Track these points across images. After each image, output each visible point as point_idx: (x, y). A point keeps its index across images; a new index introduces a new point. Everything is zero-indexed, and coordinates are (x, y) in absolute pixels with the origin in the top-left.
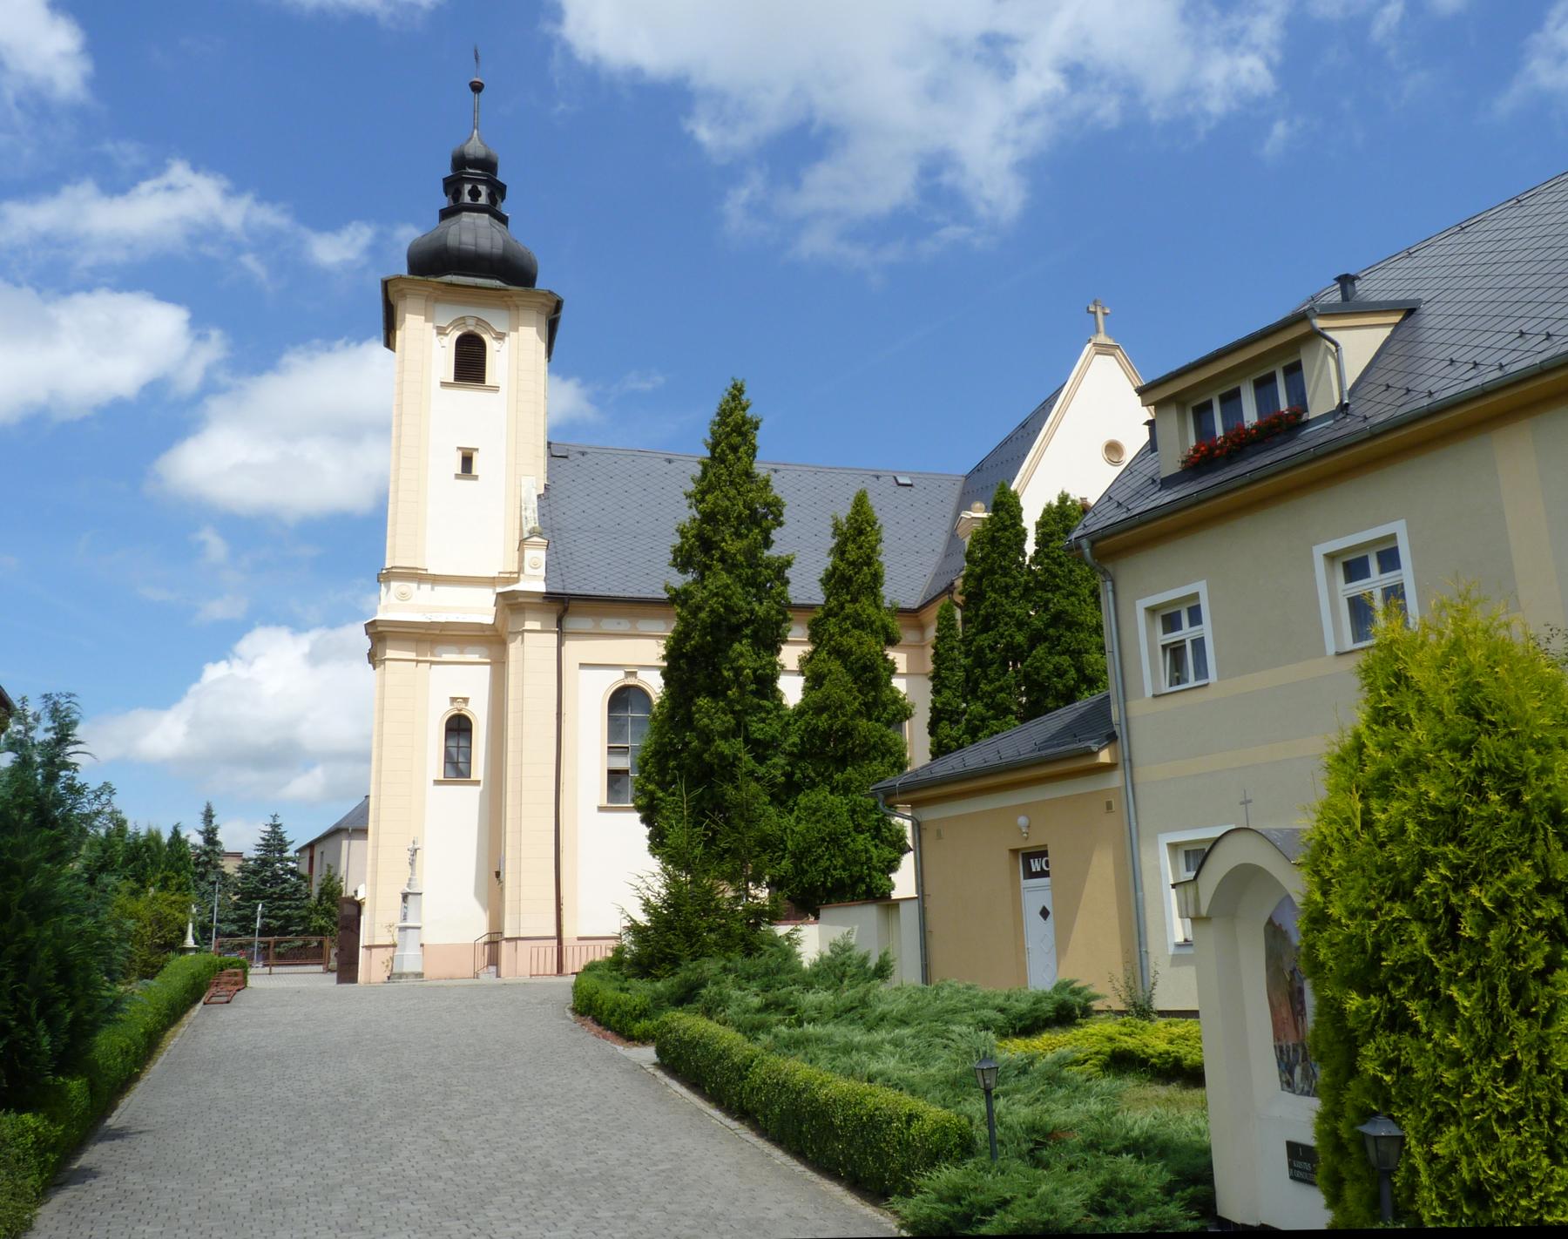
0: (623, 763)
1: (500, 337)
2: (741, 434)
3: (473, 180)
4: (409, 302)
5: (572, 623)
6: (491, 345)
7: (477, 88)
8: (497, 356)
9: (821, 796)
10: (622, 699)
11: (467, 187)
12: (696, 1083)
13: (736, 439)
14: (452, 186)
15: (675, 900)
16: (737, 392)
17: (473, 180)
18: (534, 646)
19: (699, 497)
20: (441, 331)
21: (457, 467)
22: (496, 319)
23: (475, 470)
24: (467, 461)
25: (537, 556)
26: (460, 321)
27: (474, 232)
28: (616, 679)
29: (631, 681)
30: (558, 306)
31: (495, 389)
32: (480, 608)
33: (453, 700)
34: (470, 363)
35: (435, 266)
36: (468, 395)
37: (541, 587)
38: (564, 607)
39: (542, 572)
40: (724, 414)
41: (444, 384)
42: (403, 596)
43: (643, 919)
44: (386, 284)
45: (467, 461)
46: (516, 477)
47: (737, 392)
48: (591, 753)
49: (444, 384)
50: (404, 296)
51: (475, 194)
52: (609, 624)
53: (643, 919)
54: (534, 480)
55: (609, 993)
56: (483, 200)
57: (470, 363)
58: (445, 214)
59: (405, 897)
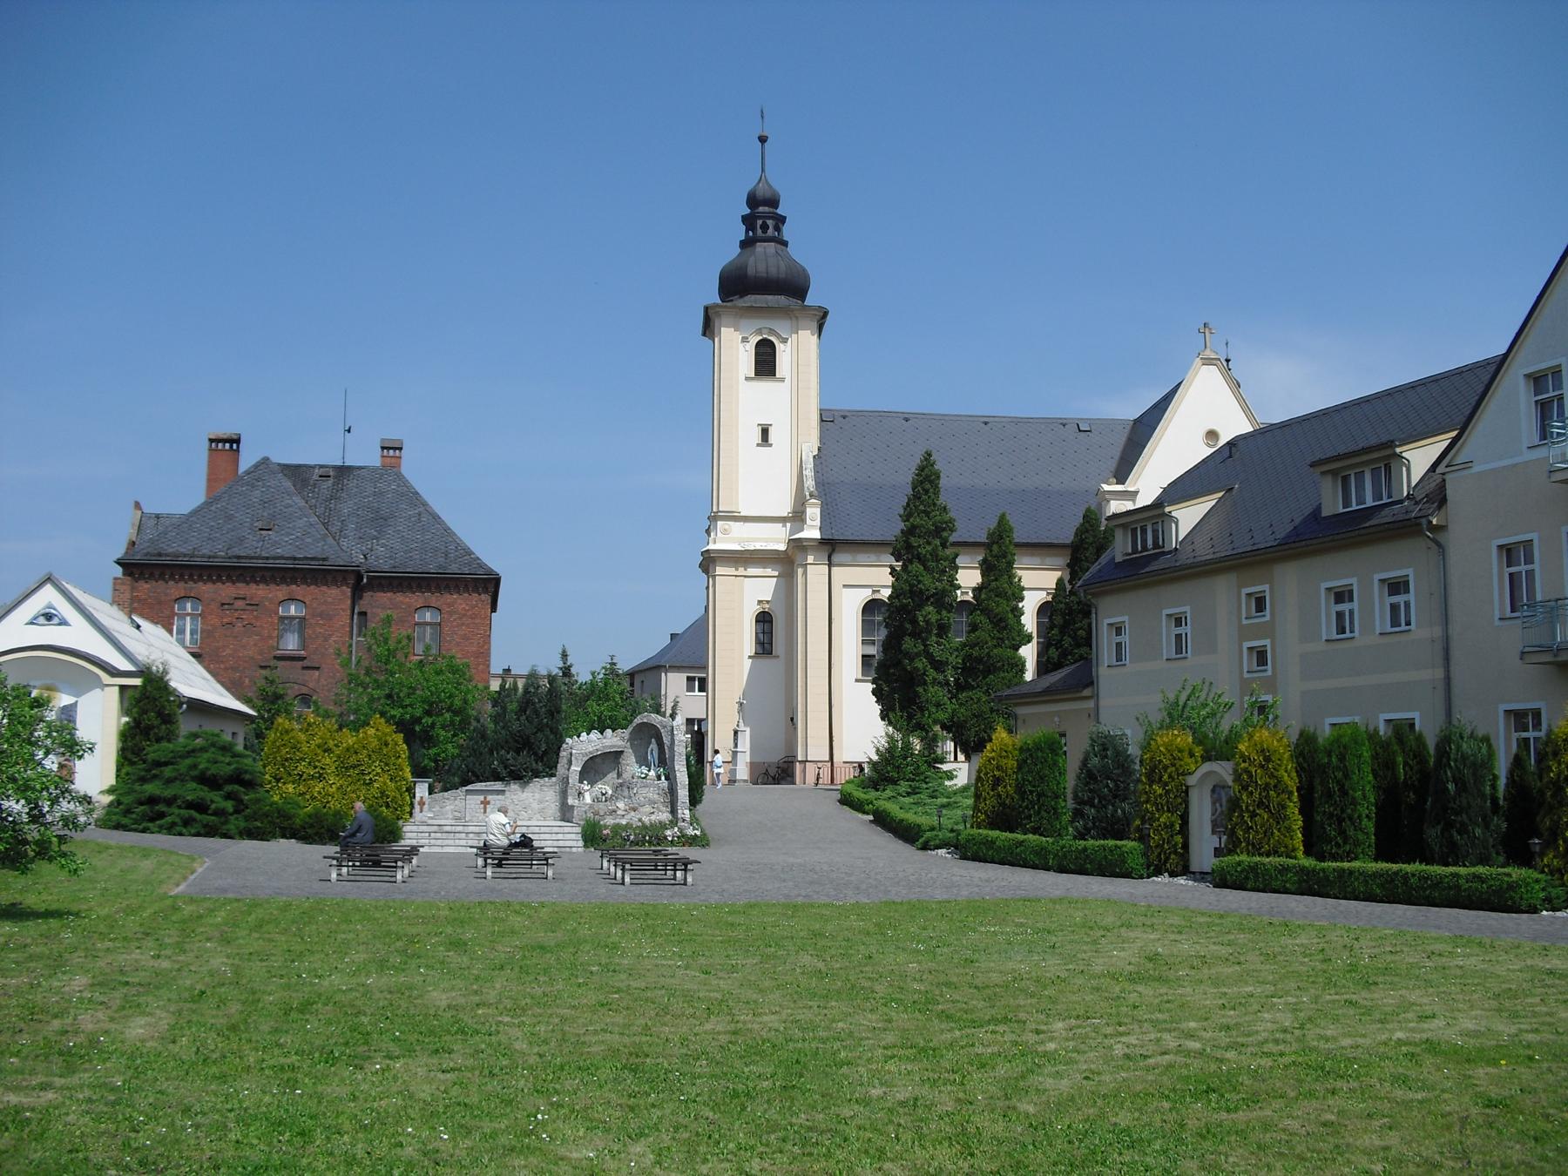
0: (872, 650)
1: (785, 341)
2: (931, 482)
3: (762, 215)
4: (724, 319)
5: (836, 558)
6: (779, 347)
7: (763, 140)
8: (784, 357)
9: (977, 694)
10: (870, 607)
11: (760, 222)
12: (976, 858)
13: (928, 486)
14: (748, 221)
15: (891, 749)
16: (1003, 517)
17: (762, 215)
18: (815, 573)
19: (906, 517)
20: (745, 340)
21: (758, 438)
22: (781, 326)
23: (772, 439)
24: (765, 432)
25: (813, 512)
26: (759, 332)
27: (764, 259)
28: (866, 595)
29: (877, 596)
30: (825, 314)
31: (782, 380)
32: (775, 538)
33: (760, 602)
34: (765, 363)
35: (738, 287)
36: (765, 385)
37: (816, 534)
38: (831, 547)
39: (818, 523)
40: (921, 469)
41: (747, 379)
42: (725, 532)
43: (875, 758)
44: (706, 309)
45: (765, 432)
46: (798, 439)
47: (1003, 517)
48: (851, 645)
49: (747, 379)
50: (719, 316)
51: (765, 227)
52: (862, 557)
53: (875, 758)
54: (811, 446)
55: (859, 794)
56: (770, 232)
57: (765, 363)
58: (745, 244)
59: (736, 733)
